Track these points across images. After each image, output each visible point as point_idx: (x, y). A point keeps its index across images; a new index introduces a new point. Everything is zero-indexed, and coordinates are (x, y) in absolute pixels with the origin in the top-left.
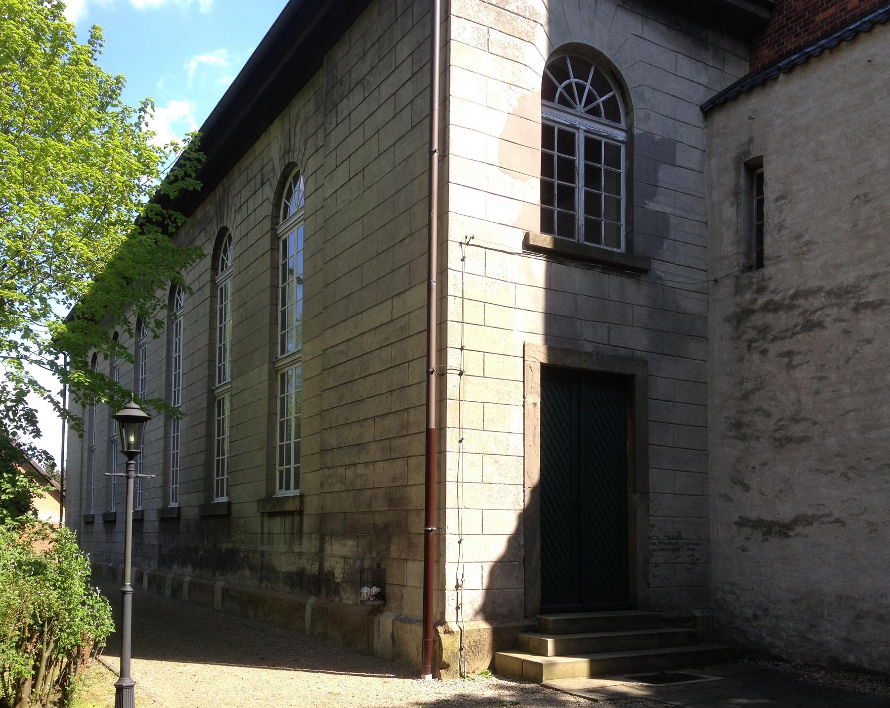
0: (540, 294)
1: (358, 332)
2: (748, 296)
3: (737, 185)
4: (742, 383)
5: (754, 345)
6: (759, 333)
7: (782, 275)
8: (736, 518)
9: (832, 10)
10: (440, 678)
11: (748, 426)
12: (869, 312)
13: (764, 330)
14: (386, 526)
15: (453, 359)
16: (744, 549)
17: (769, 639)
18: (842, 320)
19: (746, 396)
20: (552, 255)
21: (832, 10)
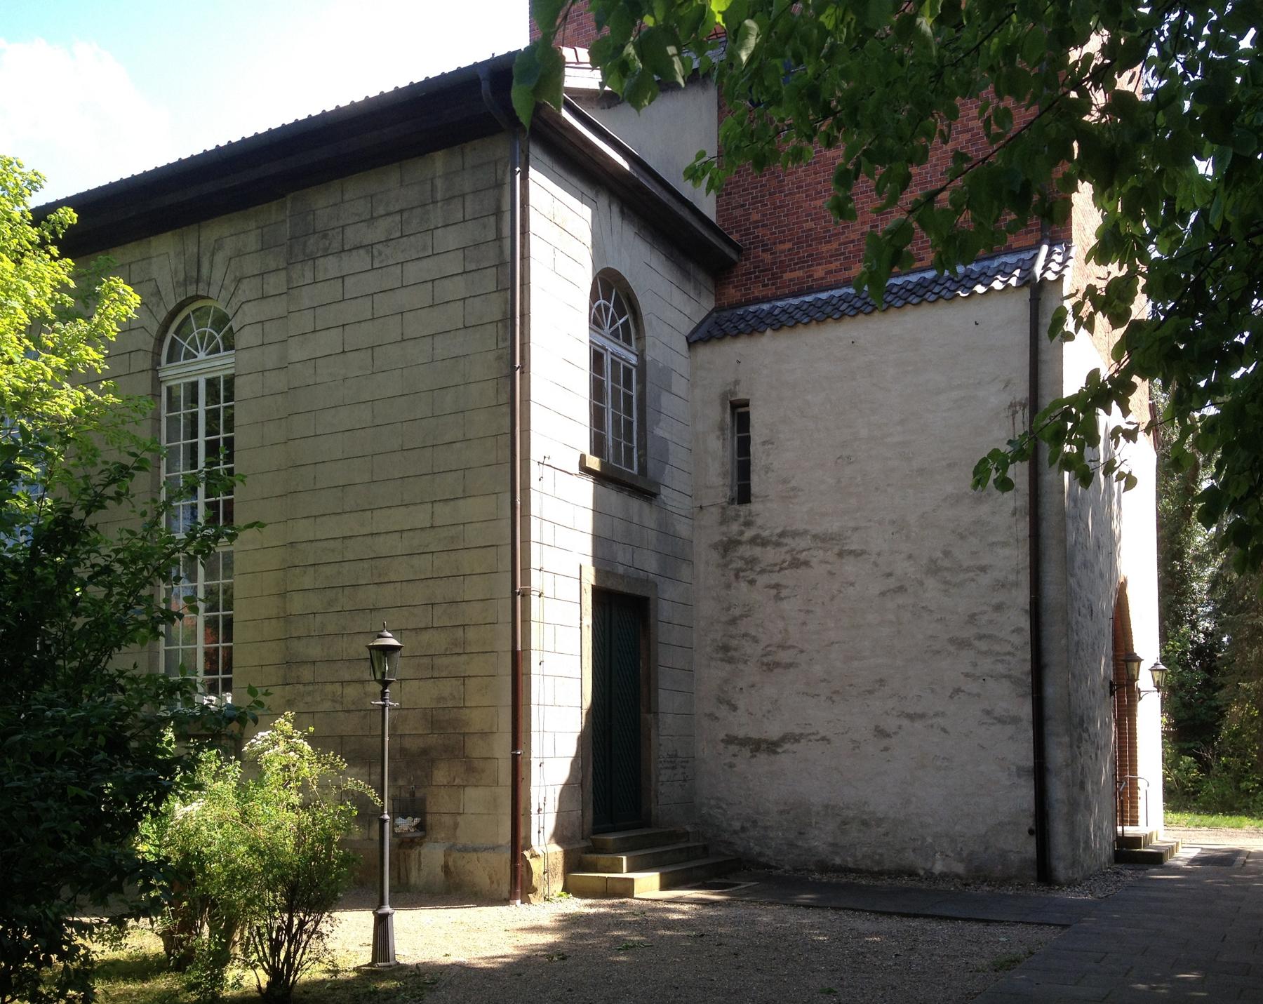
1: (367, 530)
2: (735, 527)
3: (723, 420)
4: (728, 609)
5: (742, 574)
6: (747, 563)
7: (768, 511)
8: (722, 736)
9: (799, 273)
10: (530, 902)
11: (735, 650)
12: (851, 558)
13: (752, 562)
14: (425, 752)
15: (536, 580)
16: (731, 766)
17: (757, 849)
18: (827, 562)
19: (733, 621)
20: (601, 478)
21: (799, 273)
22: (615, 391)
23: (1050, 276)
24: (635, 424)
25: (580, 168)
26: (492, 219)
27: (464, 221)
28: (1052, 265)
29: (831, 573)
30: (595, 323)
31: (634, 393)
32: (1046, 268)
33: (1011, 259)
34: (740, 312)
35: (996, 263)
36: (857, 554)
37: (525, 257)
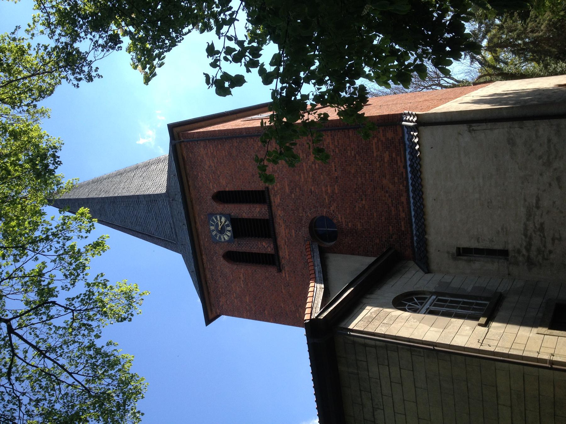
0: (509, 326)
2: (521, 259)
5: (546, 257)
7: (514, 241)
9: (402, 223)
13: (539, 251)
18: (542, 215)
21: (402, 223)
22: (448, 307)
23: (415, 119)
24: (465, 300)
25: (351, 307)
26: (367, 348)
27: (367, 362)
28: (410, 119)
29: (548, 212)
30: (415, 311)
31: (449, 299)
32: (412, 121)
33: (406, 136)
34: (416, 250)
35: (407, 143)
36: (538, 200)
37: (384, 336)
